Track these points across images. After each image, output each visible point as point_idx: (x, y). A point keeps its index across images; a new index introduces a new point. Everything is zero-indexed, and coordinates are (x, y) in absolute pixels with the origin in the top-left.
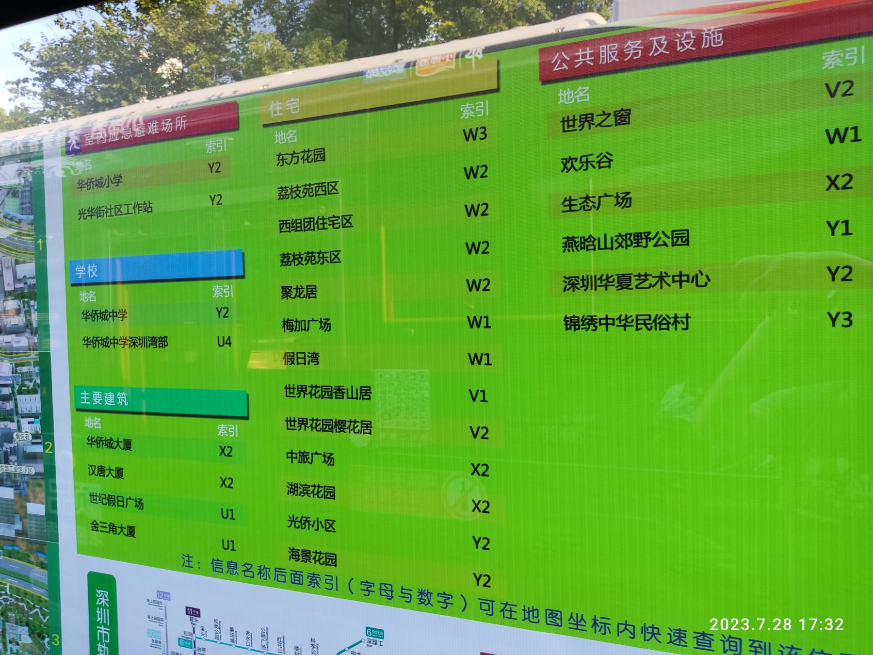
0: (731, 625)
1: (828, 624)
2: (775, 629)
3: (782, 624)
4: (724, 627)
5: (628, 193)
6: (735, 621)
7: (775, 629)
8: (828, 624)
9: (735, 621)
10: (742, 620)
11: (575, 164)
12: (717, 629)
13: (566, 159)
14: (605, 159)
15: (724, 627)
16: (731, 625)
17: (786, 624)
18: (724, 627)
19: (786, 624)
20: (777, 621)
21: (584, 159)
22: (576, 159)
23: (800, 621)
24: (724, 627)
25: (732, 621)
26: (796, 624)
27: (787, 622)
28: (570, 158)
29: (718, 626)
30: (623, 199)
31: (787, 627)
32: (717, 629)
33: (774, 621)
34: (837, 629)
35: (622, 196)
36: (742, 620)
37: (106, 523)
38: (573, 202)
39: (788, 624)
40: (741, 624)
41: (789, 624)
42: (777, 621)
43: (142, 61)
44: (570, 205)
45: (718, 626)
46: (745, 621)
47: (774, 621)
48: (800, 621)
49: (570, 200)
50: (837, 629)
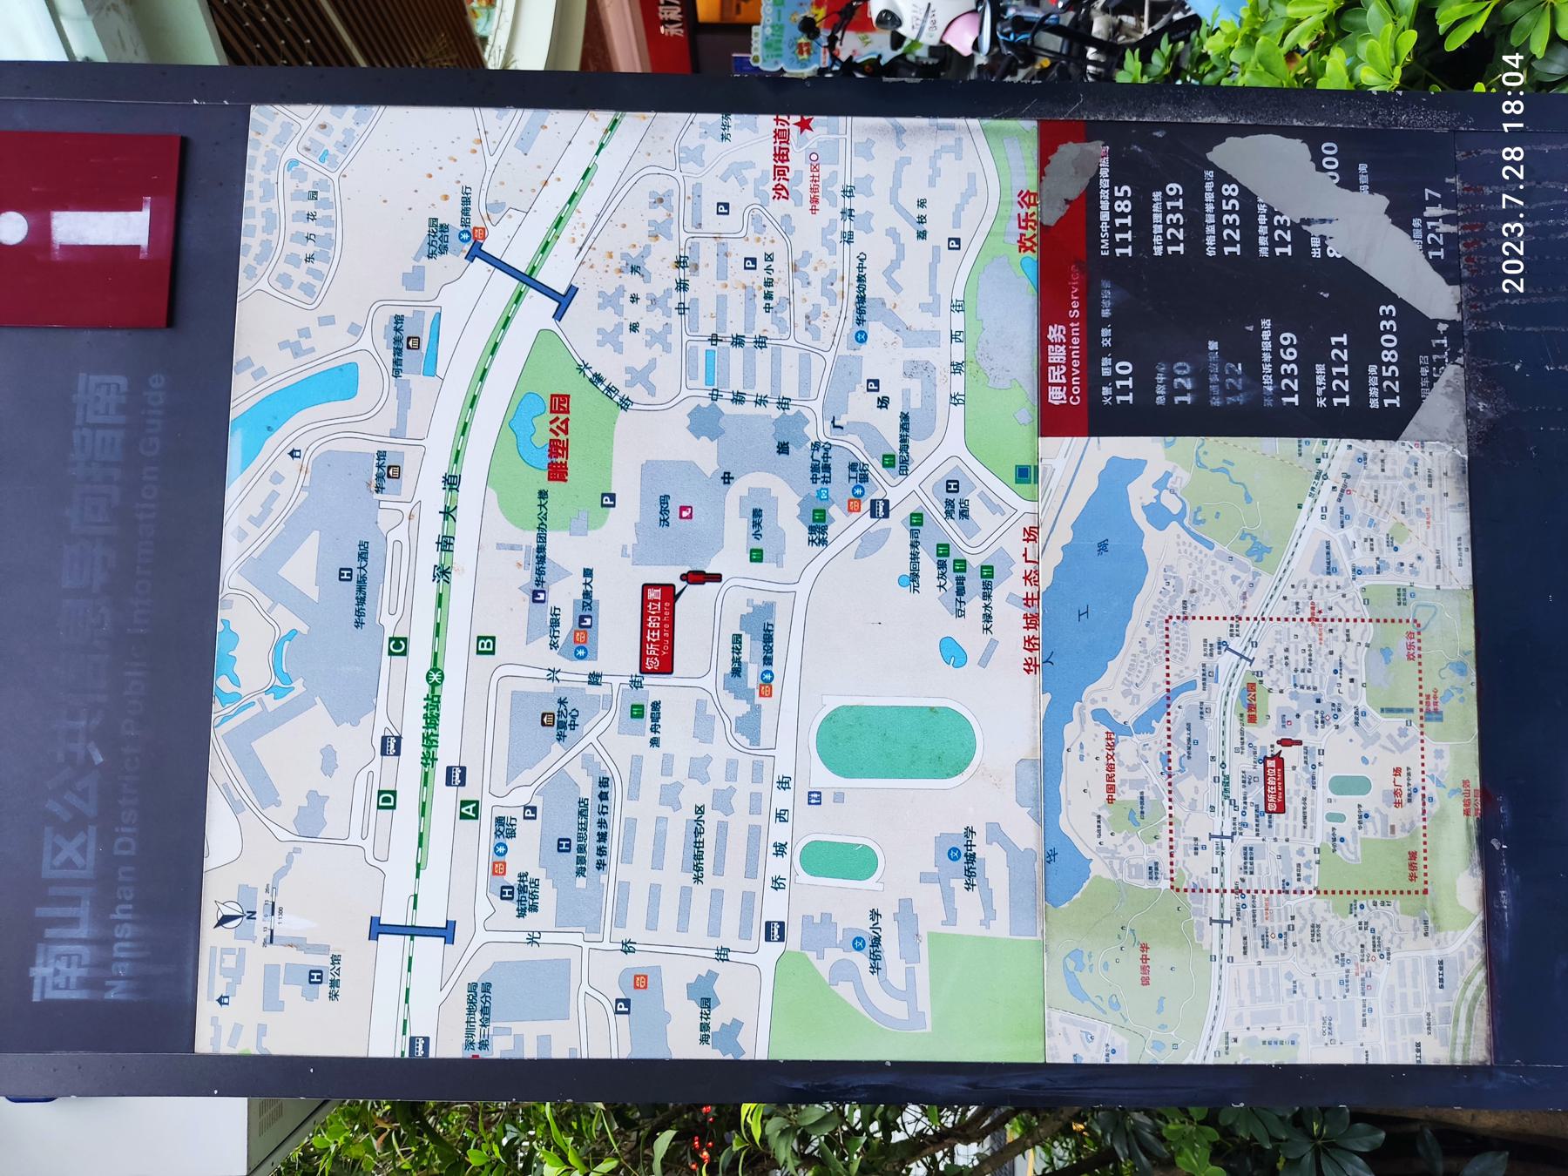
0: (1514, 255)
1: (1513, 231)
2: (1521, 176)
3: (1512, 163)
4: (1517, 267)
5: (1025, 529)
6: (1508, 248)
7: (1521, 176)
8: (1513, 231)
9: (1508, 248)
10: (1506, 234)
11: (1027, 237)
12: (1522, 280)
13: (1020, 247)
14: (1026, 199)
15: (1517, 267)
16: (1514, 255)
17: (1513, 156)
18: (1517, 267)
19: (1513, 156)
20: (1508, 172)
21: (1023, 224)
22: (1022, 235)
23: (1506, 131)
24: (1517, 267)
25: (1507, 254)
26: (1514, 138)
27: (1508, 154)
28: (1019, 241)
29: (1516, 278)
30: (1029, 535)
31: (1517, 154)
32: (1522, 280)
33: (1507, 178)
34: (1521, 252)
35: (1027, 536)
36: (1506, 234)
37: (1384, 747)
38: (1030, 596)
39: (1512, 153)
40: (1512, 236)
41: (1513, 152)
42: (1508, 172)
43: (790, 1105)
44: (1033, 599)
45: (1516, 278)
46: (1508, 230)
47: (1507, 178)
48: (1506, 131)
49: (1027, 599)
50: (1521, 252)
